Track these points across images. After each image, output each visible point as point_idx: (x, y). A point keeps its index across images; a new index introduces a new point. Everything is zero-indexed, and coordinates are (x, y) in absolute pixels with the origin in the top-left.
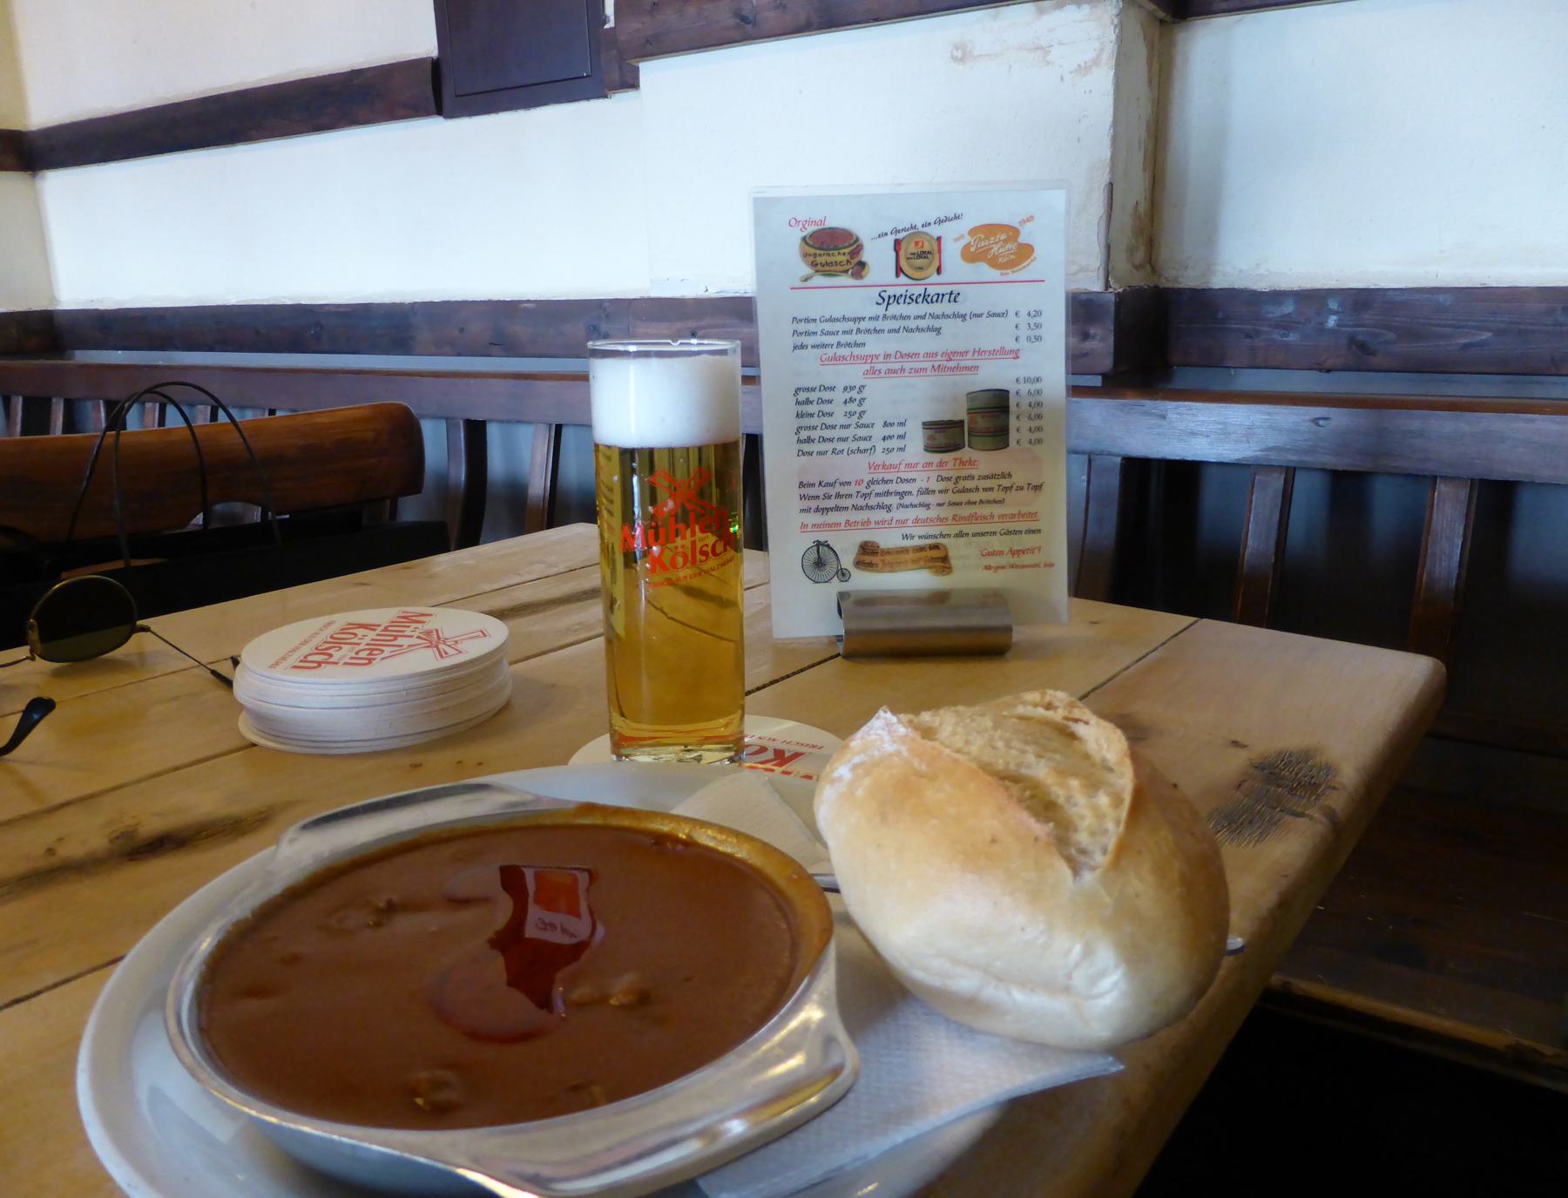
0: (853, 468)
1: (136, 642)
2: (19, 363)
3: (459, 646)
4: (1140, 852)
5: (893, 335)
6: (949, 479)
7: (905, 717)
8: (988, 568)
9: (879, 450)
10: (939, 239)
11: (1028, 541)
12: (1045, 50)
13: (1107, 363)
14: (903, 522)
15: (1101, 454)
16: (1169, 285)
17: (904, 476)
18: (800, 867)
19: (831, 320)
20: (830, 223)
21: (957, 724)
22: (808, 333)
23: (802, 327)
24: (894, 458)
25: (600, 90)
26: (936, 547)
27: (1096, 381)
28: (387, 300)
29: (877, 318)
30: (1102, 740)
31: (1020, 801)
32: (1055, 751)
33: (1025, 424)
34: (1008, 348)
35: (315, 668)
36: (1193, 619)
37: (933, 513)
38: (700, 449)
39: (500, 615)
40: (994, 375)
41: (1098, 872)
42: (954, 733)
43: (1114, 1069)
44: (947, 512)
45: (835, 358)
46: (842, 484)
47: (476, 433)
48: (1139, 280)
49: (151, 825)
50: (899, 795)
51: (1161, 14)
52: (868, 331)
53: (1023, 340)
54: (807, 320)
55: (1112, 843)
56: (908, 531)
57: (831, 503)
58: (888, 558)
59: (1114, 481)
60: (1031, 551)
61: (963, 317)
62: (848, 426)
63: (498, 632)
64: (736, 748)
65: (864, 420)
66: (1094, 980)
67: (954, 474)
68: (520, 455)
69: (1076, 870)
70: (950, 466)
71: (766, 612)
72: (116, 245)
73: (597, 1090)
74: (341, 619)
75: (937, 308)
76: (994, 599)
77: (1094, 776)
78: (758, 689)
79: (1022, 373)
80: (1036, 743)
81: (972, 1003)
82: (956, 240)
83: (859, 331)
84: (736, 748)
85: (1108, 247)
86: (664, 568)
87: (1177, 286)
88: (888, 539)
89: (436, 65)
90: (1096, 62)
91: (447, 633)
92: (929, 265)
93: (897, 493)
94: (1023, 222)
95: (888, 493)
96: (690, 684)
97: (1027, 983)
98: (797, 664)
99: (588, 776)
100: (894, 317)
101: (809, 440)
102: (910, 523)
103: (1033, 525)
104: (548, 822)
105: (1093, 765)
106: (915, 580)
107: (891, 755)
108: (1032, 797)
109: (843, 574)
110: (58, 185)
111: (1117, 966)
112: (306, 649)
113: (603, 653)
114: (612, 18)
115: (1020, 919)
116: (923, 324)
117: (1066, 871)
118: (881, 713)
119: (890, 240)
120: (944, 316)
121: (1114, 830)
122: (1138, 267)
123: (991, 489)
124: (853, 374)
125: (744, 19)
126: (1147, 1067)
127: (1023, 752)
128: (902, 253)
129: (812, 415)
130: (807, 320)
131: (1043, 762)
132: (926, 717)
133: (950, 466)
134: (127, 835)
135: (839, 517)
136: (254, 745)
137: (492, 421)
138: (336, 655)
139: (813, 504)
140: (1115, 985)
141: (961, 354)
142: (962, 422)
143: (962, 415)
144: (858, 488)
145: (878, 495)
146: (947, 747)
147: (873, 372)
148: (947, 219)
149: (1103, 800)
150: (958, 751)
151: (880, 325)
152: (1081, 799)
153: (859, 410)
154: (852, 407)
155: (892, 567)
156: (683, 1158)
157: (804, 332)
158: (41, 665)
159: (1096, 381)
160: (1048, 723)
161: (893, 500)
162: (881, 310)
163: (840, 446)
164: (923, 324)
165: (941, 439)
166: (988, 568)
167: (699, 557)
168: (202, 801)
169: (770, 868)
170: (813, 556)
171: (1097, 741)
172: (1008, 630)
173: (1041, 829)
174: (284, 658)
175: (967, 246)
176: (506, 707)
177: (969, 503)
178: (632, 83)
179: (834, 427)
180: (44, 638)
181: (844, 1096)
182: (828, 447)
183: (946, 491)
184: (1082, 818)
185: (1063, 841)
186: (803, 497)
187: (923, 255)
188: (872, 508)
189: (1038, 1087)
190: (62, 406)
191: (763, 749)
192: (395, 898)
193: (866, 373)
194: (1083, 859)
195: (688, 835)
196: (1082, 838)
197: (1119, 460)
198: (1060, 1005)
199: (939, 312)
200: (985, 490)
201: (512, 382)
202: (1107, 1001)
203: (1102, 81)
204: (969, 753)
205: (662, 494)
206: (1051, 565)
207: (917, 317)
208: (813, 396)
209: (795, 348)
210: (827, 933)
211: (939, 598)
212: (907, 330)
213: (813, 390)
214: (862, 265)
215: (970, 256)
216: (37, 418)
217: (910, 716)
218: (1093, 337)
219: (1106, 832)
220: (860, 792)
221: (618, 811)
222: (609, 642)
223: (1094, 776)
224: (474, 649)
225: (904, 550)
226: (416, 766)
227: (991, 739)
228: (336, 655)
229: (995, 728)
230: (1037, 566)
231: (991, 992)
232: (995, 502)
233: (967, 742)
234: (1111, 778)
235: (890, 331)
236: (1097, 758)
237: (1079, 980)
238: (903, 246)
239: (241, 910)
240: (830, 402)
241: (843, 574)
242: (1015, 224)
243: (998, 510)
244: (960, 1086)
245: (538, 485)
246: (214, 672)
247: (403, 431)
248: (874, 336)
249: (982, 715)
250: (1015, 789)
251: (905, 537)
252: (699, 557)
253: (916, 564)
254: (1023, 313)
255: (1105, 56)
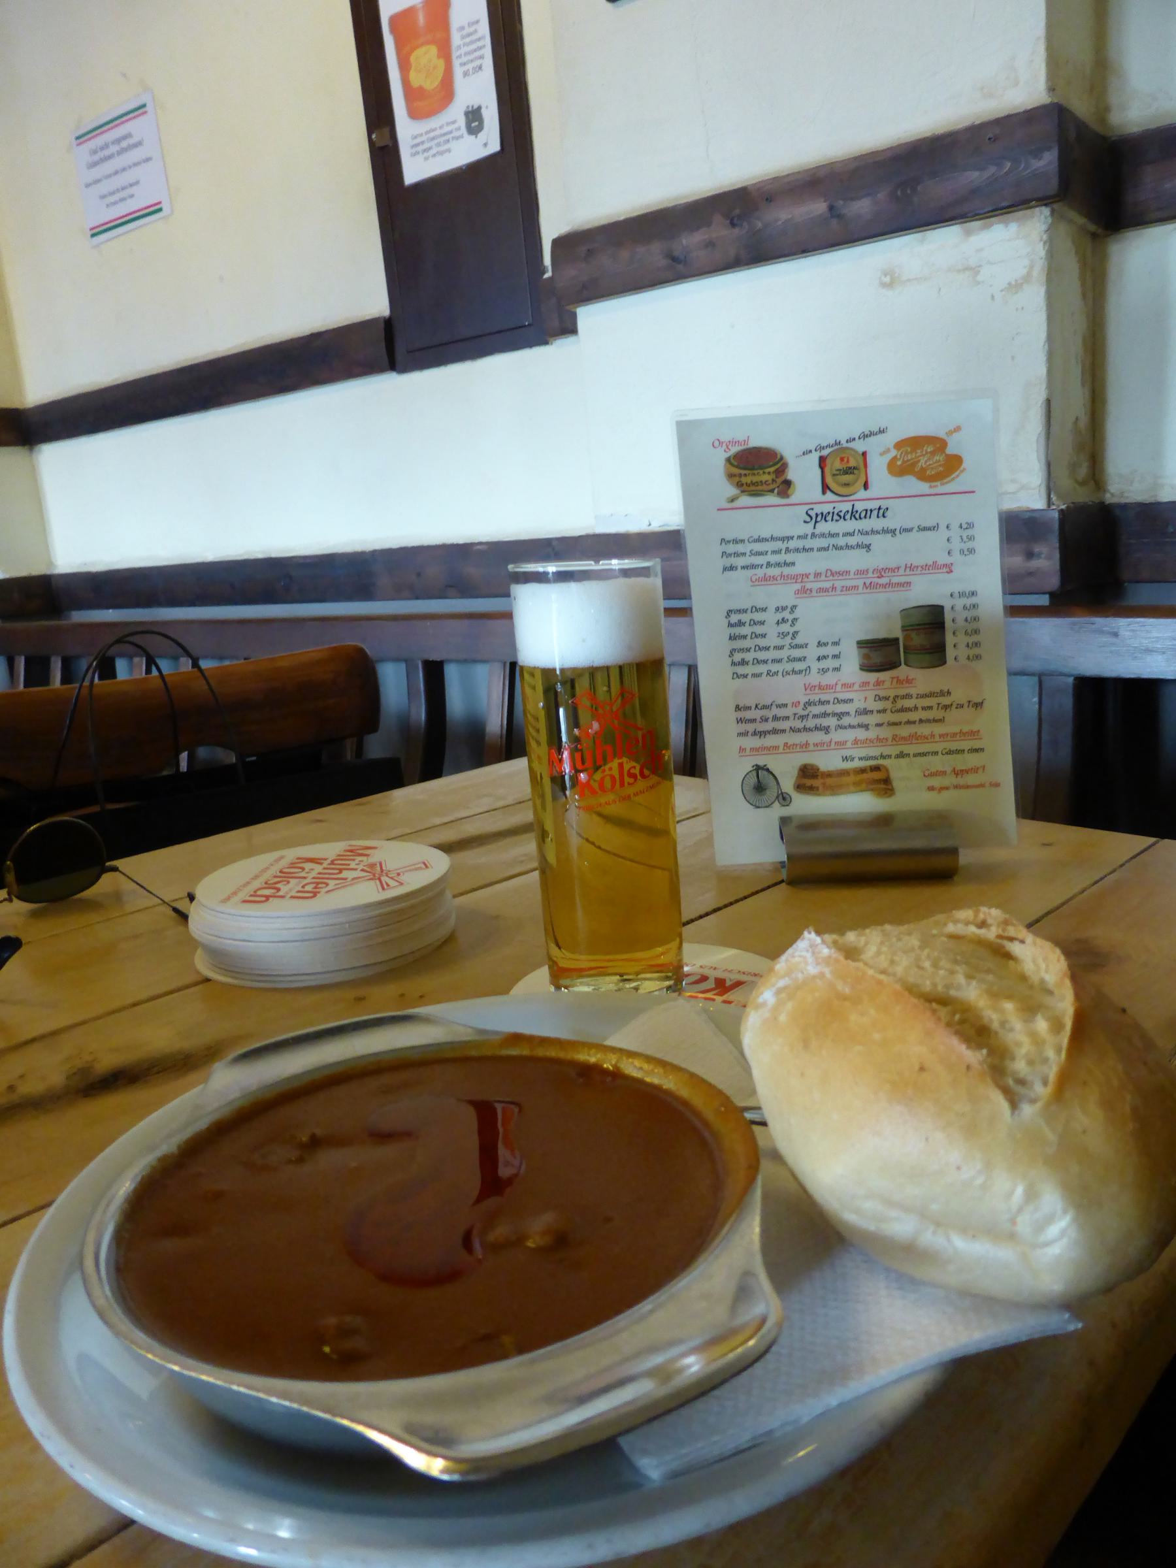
0: (788, 690)
1: (106, 882)
2: (20, 625)
3: (402, 878)
4: (1085, 1083)
5: (823, 553)
6: (887, 698)
7: (829, 938)
8: (931, 789)
9: (814, 670)
10: (864, 454)
11: (973, 760)
12: (974, 270)
13: (1054, 582)
14: (841, 744)
15: (1052, 674)
16: (1115, 500)
17: (841, 696)
18: (728, 1098)
19: (759, 540)
20: (753, 443)
21: (882, 943)
22: (737, 555)
23: (731, 548)
24: (830, 679)
25: (542, 339)
26: (876, 768)
27: (1044, 600)
28: (349, 549)
29: (805, 537)
30: (1041, 960)
31: (949, 1025)
32: (989, 971)
33: (962, 639)
34: (941, 562)
35: (264, 903)
36: (1152, 840)
37: (872, 733)
38: (621, 667)
39: (448, 848)
40: (925, 591)
41: (1039, 1105)
42: (879, 953)
43: (1071, 1327)
44: (886, 733)
45: (766, 579)
46: (779, 706)
47: (434, 673)
48: (1083, 496)
49: (107, 1062)
50: (822, 1020)
51: (1092, 228)
52: (797, 550)
53: (956, 553)
54: (736, 541)
55: (1052, 1072)
56: (848, 753)
57: (769, 726)
58: (829, 781)
59: (1067, 702)
60: (975, 770)
61: (893, 532)
62: (781, 648)
63: (440, 863)
64: (676, 978)
65: (799, 640)
66: (1040, 1226)
67: (892, 693)
68: (476, 694)
69: (1014, 1104)
70: (887, 684)
71: (709, 840)
72: (111, 513)
73: (507, 1340)
74: (291, 854)
75: (865, 524)
76: (939, 820)
77: (1032, 1001)
78: (701, 917)
79: (957, 588)
80: (967, 963)
81: (909, 1250)
82: (882, 454)
83: (788, 550)
84: (676, 978)
85: (1049, 465)
86: (593, 792)
87: (1123, 501)
88: (828, 761)
89: (388, 325)
90: (1027, 278)
91: (390, 865)
92: (856, 481)
93: (835, 714)
94: (950, 433)
95: (825, 715)
96: (628, 913)
97: (968, 1229)
98: (738, 891)
99: (528, 1007)
100: (823, 535)
101: (743, 663)
102: (849, 745)
103: (976, 744)
104: (474, 1053)
105: (1031, 987)
106: (857, 803)
107: (814, 977)
108: (962, 1022)
109: (784, 799)
110: (54, 457)
111: (1065, 1212)
112: (257, 884)
113: (538, 885)
114: (550, 268)
115: (954, 1155)
116: (852, 541)
117: (1005, 1105)
118: (806, 933)
119: (815, 457)
120: (873, 532)
121: (1055, 1058)
122: (1082, 484)
123: (931, 708)
124: (785, 594)
125: (675, 259)
126: (1114, 1326)
127: (952, 972)
128: (827, 470)
129: (745, 637)
130: (736, 541)
131: (974, 983)
132: (851, 937)
133: (887, 684)
134: (84, 1071)
135: (771, 741)
136: (208, 980)
137: (450, 661)
138: (284, 889)
139: (751, 727)
140: (1063, 1233)
141: (893, 570)
142: (897, 640)
143: (898, 633)
144: (795, 710)
145: (815, 716)
146: (871, 967)
147: (804, 592)
148: (872, 434)
149: (1042, 1025)
150: (883, 972)
151: (809, 543)
152: (1018, 1025)
153: (792, 630)
154: (785, 627)
155: (834, 790)
156: (588, 1420)
157: (732, 554)
158: (21, 907)
159: (1044, 600)
160: (980, 942)
161: (831, 722)
162: (809, 529)
163: (774, 668)
164: (852, 541)
165: (877, 658)
166: (931, 789)
167: (627, 779)
168: (157, 1036)
169: (698, 1100)
170: (753, 780)
171: (1034, 961)
172: (954, 852)
173: (975, 1057)
174: (235, 893)
175: (894, 459)
176: (450, 939)
177: (909, 722)
178: (569, 329)
179: (767, 649)
180: (21, 879)
181: (767, 1350)
182: (763, 669)
183: (884, 711)
184: (1018, 1044)
185: (998, 1068)
186: (740, 721)
187: (849, 471)
188: (810, 730)
189: (986, 1346)
190: (59, 664)
191: (704, 978)
192: (319, 1132)
193: (797, 592)
194: (1019, 1089)
195: (615, 1066)
196: (1020, 1066)
197: (1071, 680)
198: (1004, 1253)
199: (869, 529)
200: (924, 708)
201: (466, 622)
202: (1055, 1250)
203: (1035, 297)
204: (894, 975)
205: (584, 716)
206: (997, 785)
207: (845, 535)
208: (745, 618)
209: (725, 569)
210: (753, 1168)
211: (883, 821)
212: (836, 547)
213: (745, 611)
214: (788, 483)
215: (898, 469)
216: (37, 672)
217: (835, 937)
218: (1039, 556)
219: (1045, 1060)
220: (783, 1018)
221: (544, 1041)
222: (543, 872)
223: (1032, 1001)
224: (415, 881)
225: (844, 773)
226: (360, 999)
227: (918, 959)
228: (284, 889)
229: (922, 948)
230: (982, 786)
231: (930, 1238)
232: (935, 721)
233: (892, 962)
234: (1048, 1000)
235: (819, 550)
236: (1035, 979)
237: (1024, 1225)
238: (828, 462)
239: (169, 1147)
240: (762, 623)
241: (784, 799)
242: (941, 434)
243: (938, 729)
244: (898, 1344)
245: (495, 723)
246: (175, 910)
247: (360, 672)
248: (803, 555)
249: (910, 934)
250: (943, 1012)
251: (845, 759)
252: (627, 779)
253: (859, 787)
254: (955, 526)
255: (1035, 273)
